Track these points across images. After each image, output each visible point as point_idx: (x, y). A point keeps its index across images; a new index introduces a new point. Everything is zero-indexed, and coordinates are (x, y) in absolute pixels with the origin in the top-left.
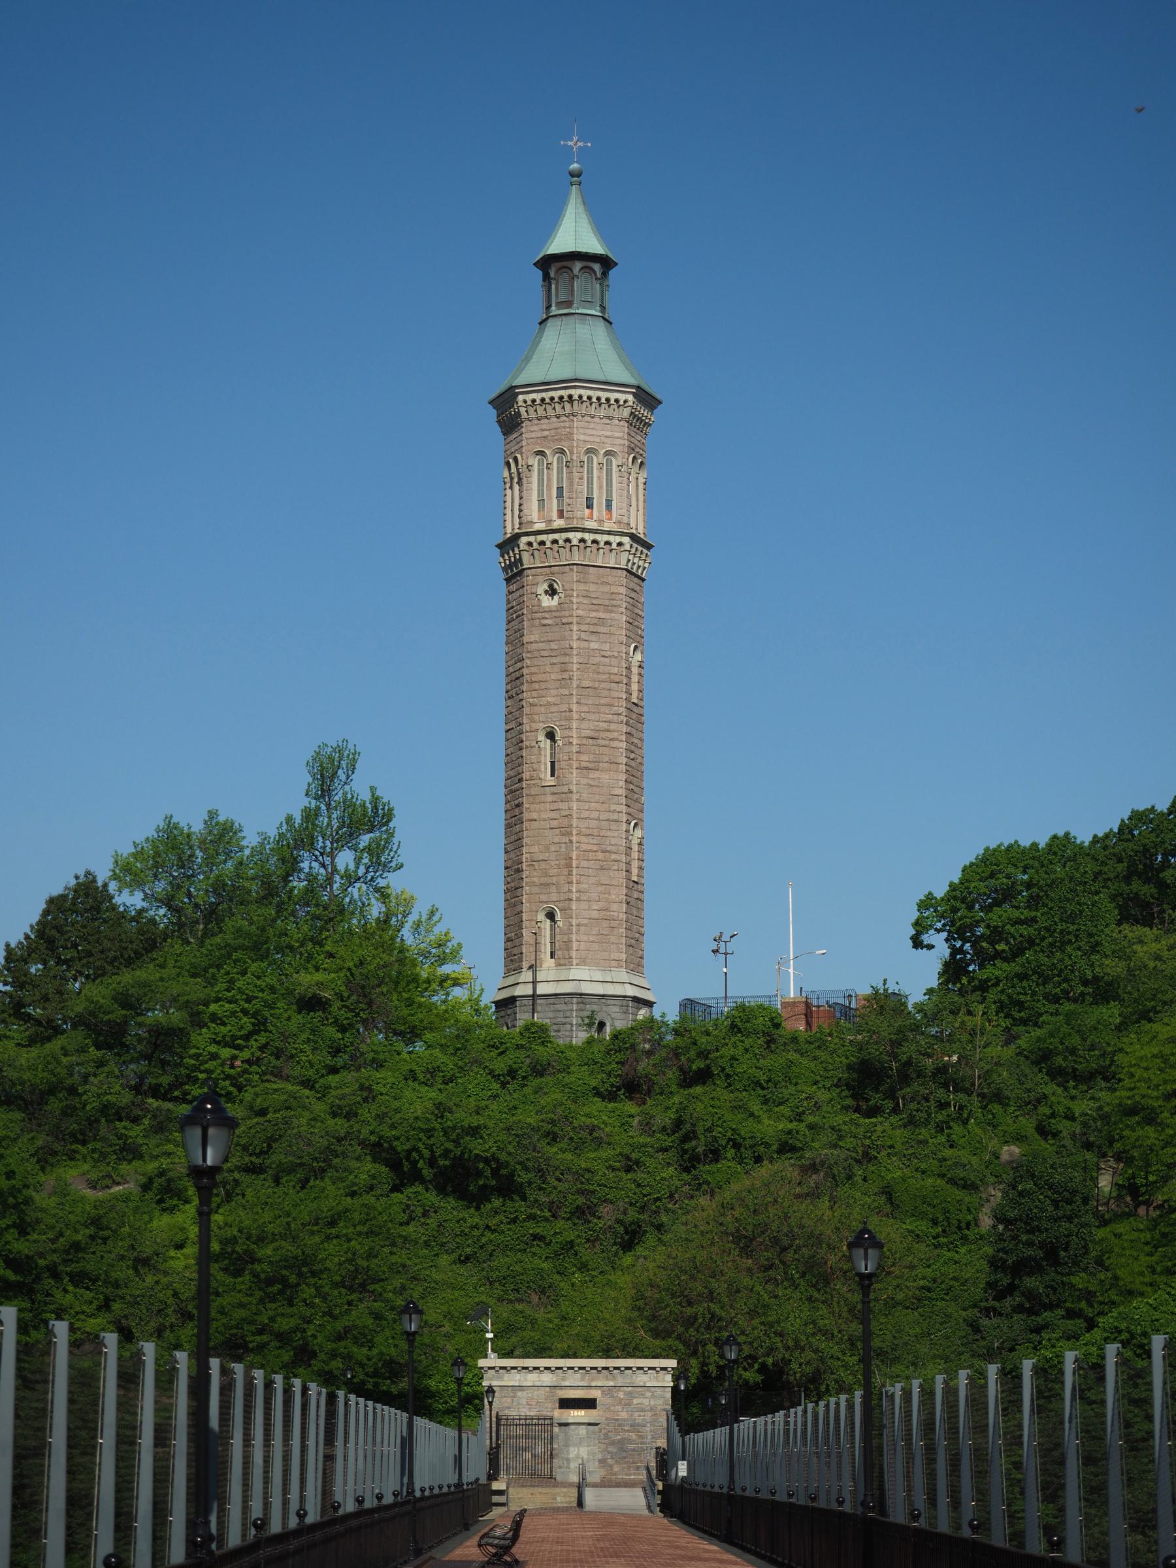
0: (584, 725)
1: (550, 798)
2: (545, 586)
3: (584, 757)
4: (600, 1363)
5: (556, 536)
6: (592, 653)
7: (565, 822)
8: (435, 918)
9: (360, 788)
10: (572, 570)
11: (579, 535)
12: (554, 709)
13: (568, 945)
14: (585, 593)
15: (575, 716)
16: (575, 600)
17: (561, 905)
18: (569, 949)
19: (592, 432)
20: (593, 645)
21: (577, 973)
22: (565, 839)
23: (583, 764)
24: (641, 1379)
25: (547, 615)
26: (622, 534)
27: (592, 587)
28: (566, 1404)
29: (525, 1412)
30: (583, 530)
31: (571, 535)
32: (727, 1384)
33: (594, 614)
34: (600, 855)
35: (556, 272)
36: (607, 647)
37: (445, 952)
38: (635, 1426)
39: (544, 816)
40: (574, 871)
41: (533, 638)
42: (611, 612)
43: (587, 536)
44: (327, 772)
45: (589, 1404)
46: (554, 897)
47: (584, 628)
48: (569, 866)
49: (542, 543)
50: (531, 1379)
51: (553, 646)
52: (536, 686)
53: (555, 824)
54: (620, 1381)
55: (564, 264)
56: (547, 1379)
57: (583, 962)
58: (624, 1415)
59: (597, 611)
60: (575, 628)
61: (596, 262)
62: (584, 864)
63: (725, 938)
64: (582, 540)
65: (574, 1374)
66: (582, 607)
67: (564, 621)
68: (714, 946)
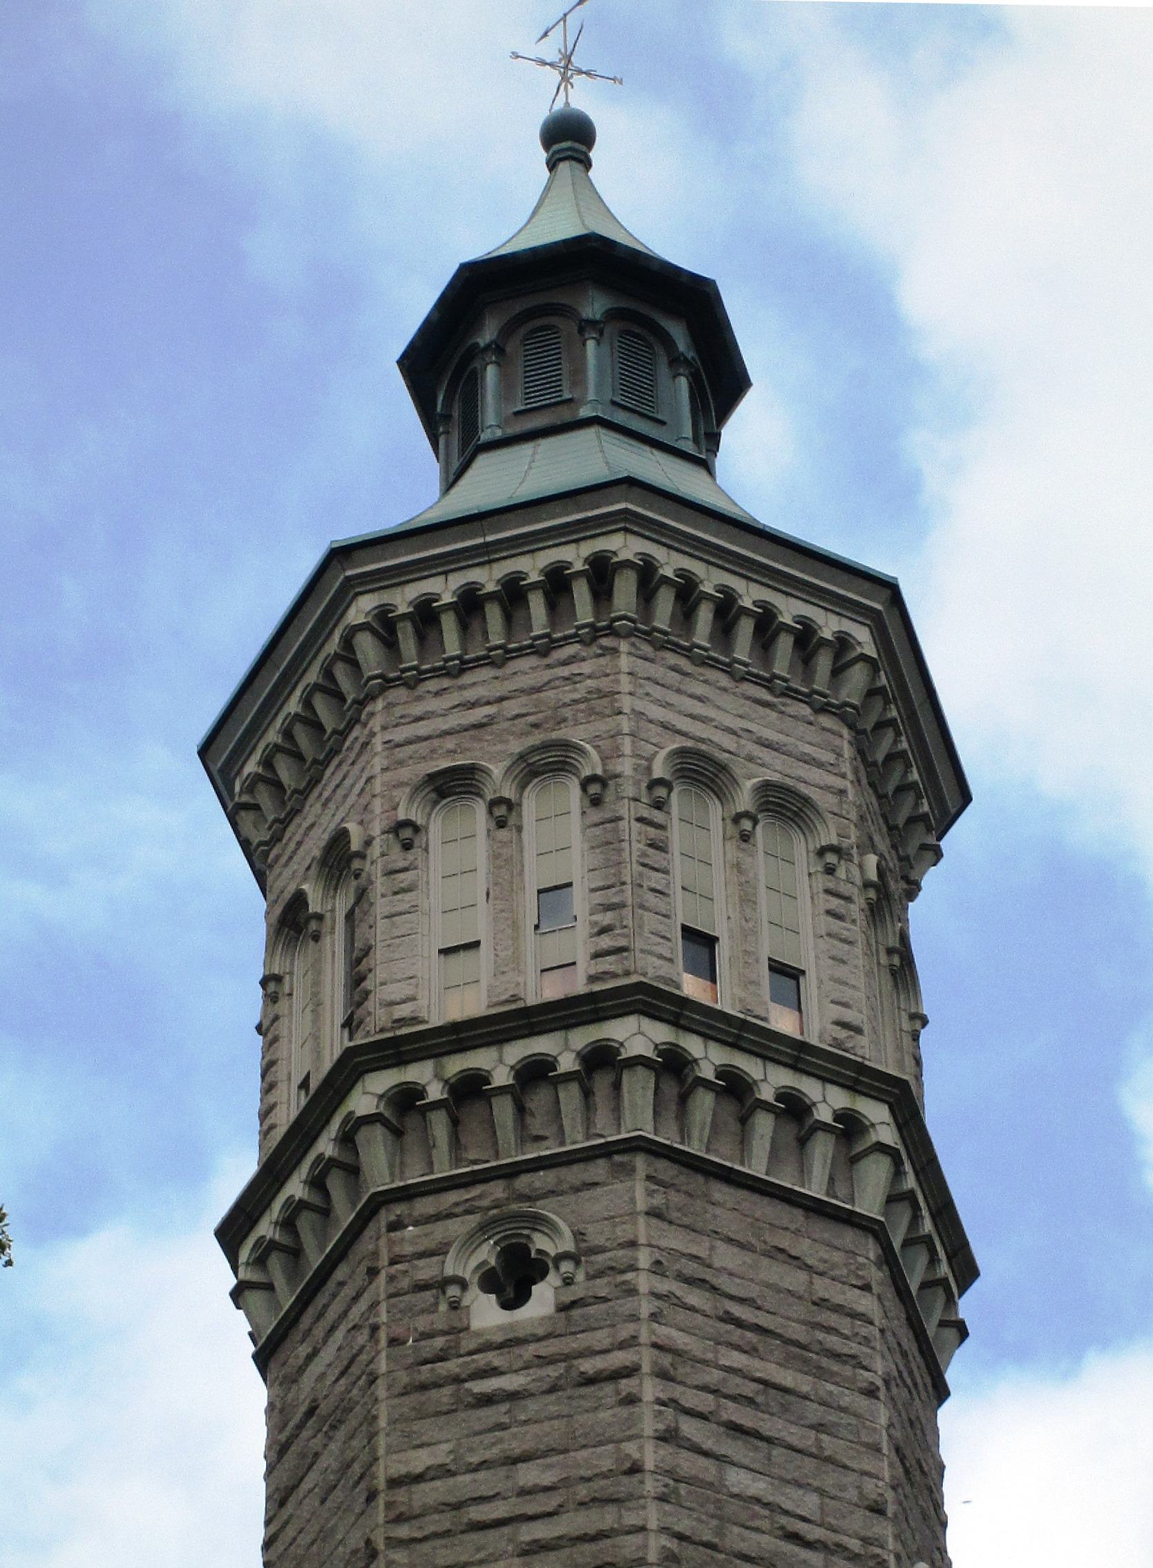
6: (733, 1507)
10: (630, 1171)
11: (661, 1033)
14: (691, 1269)
16: (644, 1282)
19: (699, 709)
20: (737, 1480)
25: (494, 1358)
26: (860, 1078)
27: (726, 1257)
33: (737, 1359)
35: (507, 331)
36: (809, 1503)
41: (420, 1460)
42: (821, 1373)
51: (529, 1475)
55: (538, 323)
59: (751, 1351)
61: (875, 1095)
66: (682, 1316)
67: (589, 1366)
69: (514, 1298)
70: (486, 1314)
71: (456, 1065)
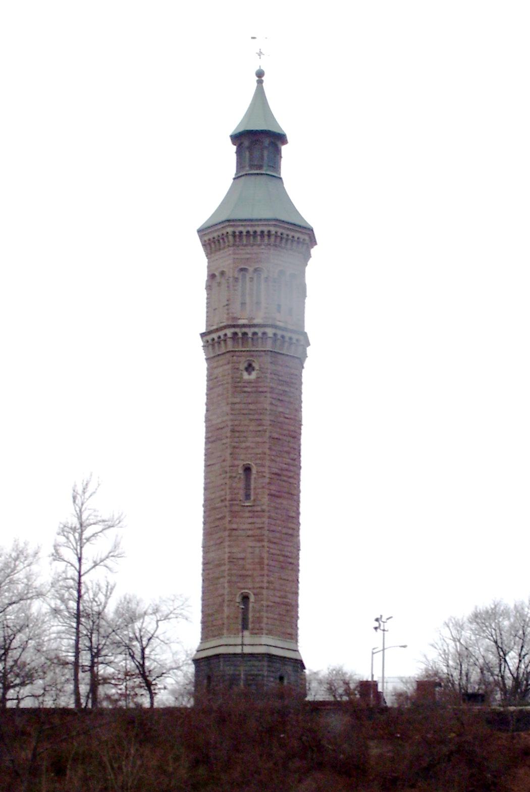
0: (273, 465)
1: (247, 515)
3: (273, 487)
7: (258, 532)
11: (274, 331)
15: (268, 457)
17: (255, 591)
20: (281, 409)
22: (259, 544)
23: (273, 492)
34: (282, 559)
39: (244, 527)
40: (266, 567)
41: (237, 400)
46: (250, 585)
47: (274, 396)
51: (251, 407)
52: (237, 434)
53: (250, 533)
63: (384, 619)
69: (250, 374)
70: (246, 376)
71: (244, 330)
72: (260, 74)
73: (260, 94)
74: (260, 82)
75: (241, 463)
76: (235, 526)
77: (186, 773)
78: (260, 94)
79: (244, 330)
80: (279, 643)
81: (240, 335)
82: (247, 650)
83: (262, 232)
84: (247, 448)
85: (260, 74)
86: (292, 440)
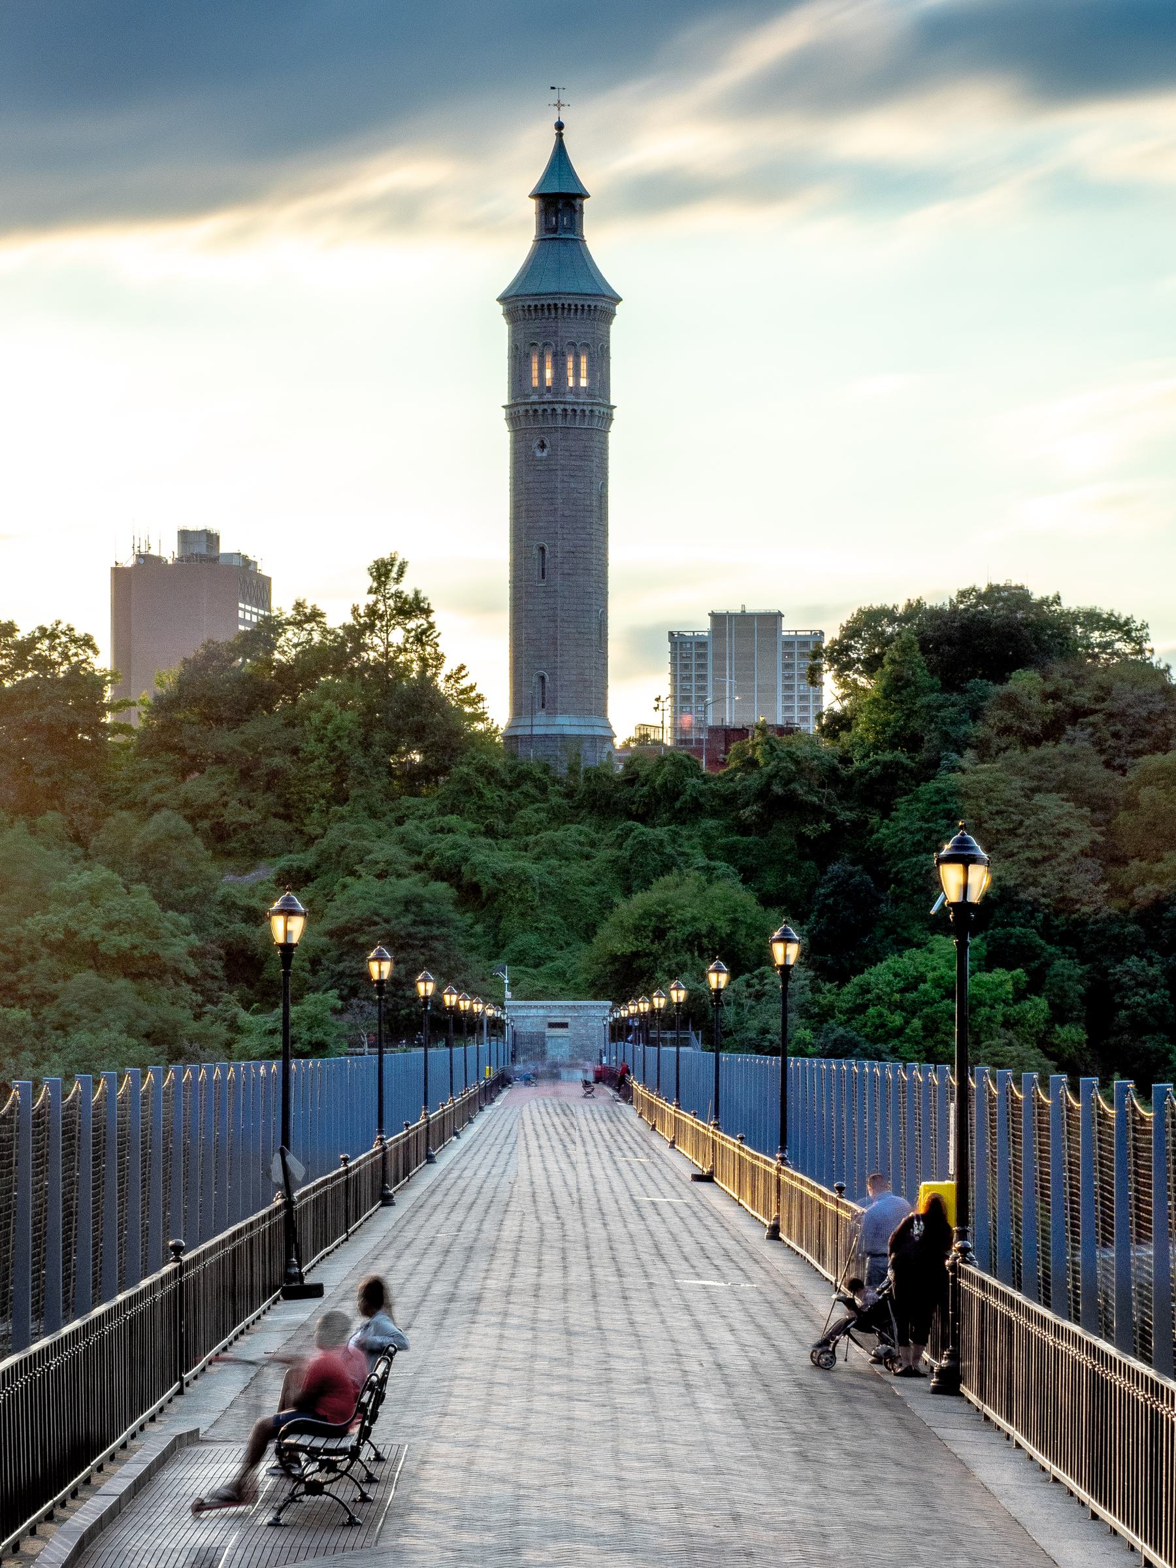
1: (543, 595)
2: (538, 442)
3: (566, 566)
4: (571, 1003)
5: (546, 407)
8: (463, 673)
9: (407, 586)
11: (562, 406)
12: (543, 531)
13: (554, 699)
15: (560, 537)
18: (555, 702)
20: (573, 485)
21: (561, 720)
22: (552, 624)
24: (592, 1012)
28: (552, 1025)
29: (529, 1029)
30: (565, 403)
31: (556, 406)
32: (876, 650)
34: (577, 636)
36: (582, 485)
37: (470, 696)
38: (589, 1038)
43: (567, 407)
44: (382, 571)
45: (564, 1025)
46: (544, 665)
48: (555, 644)
49: (536, 411)
50: (533, 1012)
53: (544, 614)
54: (581, 1013)
56: (541, 1012)
57: (565, 712)
58: (583, 1031)
60: (559, 473)
62: (566, 642)
64: (565, 410)
65: (558, 1008)
68: (655, 704)
70: (539, 454)
71: (534, 407)
72: (560, 126)
73: (560, 150)
74: (560, 136)
75: (535, 543)
76: (530, 607)
77: (882, 819)
78: (560, 150)
79: (534, 407)
80: (575, 721)
81: (540, 412)
82: (538, 731)
83: (536, 306)
84: (541, 528)
85: (560, 126)
86: (588, 514)
